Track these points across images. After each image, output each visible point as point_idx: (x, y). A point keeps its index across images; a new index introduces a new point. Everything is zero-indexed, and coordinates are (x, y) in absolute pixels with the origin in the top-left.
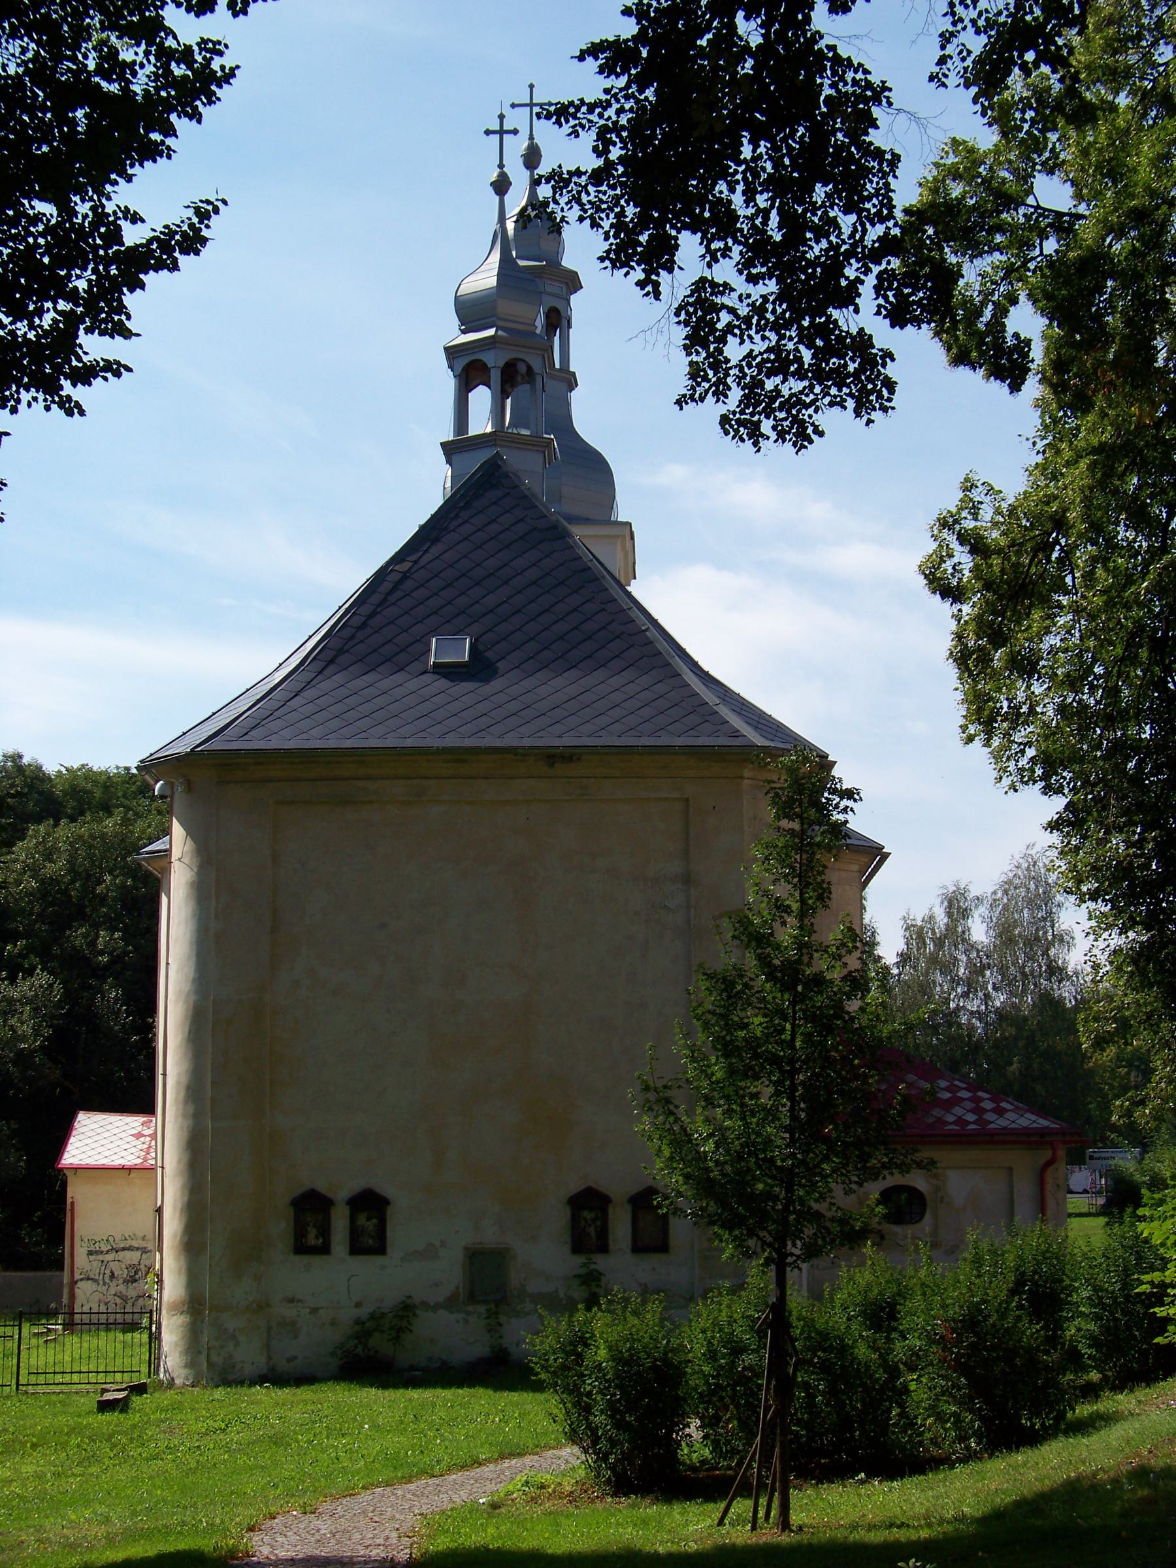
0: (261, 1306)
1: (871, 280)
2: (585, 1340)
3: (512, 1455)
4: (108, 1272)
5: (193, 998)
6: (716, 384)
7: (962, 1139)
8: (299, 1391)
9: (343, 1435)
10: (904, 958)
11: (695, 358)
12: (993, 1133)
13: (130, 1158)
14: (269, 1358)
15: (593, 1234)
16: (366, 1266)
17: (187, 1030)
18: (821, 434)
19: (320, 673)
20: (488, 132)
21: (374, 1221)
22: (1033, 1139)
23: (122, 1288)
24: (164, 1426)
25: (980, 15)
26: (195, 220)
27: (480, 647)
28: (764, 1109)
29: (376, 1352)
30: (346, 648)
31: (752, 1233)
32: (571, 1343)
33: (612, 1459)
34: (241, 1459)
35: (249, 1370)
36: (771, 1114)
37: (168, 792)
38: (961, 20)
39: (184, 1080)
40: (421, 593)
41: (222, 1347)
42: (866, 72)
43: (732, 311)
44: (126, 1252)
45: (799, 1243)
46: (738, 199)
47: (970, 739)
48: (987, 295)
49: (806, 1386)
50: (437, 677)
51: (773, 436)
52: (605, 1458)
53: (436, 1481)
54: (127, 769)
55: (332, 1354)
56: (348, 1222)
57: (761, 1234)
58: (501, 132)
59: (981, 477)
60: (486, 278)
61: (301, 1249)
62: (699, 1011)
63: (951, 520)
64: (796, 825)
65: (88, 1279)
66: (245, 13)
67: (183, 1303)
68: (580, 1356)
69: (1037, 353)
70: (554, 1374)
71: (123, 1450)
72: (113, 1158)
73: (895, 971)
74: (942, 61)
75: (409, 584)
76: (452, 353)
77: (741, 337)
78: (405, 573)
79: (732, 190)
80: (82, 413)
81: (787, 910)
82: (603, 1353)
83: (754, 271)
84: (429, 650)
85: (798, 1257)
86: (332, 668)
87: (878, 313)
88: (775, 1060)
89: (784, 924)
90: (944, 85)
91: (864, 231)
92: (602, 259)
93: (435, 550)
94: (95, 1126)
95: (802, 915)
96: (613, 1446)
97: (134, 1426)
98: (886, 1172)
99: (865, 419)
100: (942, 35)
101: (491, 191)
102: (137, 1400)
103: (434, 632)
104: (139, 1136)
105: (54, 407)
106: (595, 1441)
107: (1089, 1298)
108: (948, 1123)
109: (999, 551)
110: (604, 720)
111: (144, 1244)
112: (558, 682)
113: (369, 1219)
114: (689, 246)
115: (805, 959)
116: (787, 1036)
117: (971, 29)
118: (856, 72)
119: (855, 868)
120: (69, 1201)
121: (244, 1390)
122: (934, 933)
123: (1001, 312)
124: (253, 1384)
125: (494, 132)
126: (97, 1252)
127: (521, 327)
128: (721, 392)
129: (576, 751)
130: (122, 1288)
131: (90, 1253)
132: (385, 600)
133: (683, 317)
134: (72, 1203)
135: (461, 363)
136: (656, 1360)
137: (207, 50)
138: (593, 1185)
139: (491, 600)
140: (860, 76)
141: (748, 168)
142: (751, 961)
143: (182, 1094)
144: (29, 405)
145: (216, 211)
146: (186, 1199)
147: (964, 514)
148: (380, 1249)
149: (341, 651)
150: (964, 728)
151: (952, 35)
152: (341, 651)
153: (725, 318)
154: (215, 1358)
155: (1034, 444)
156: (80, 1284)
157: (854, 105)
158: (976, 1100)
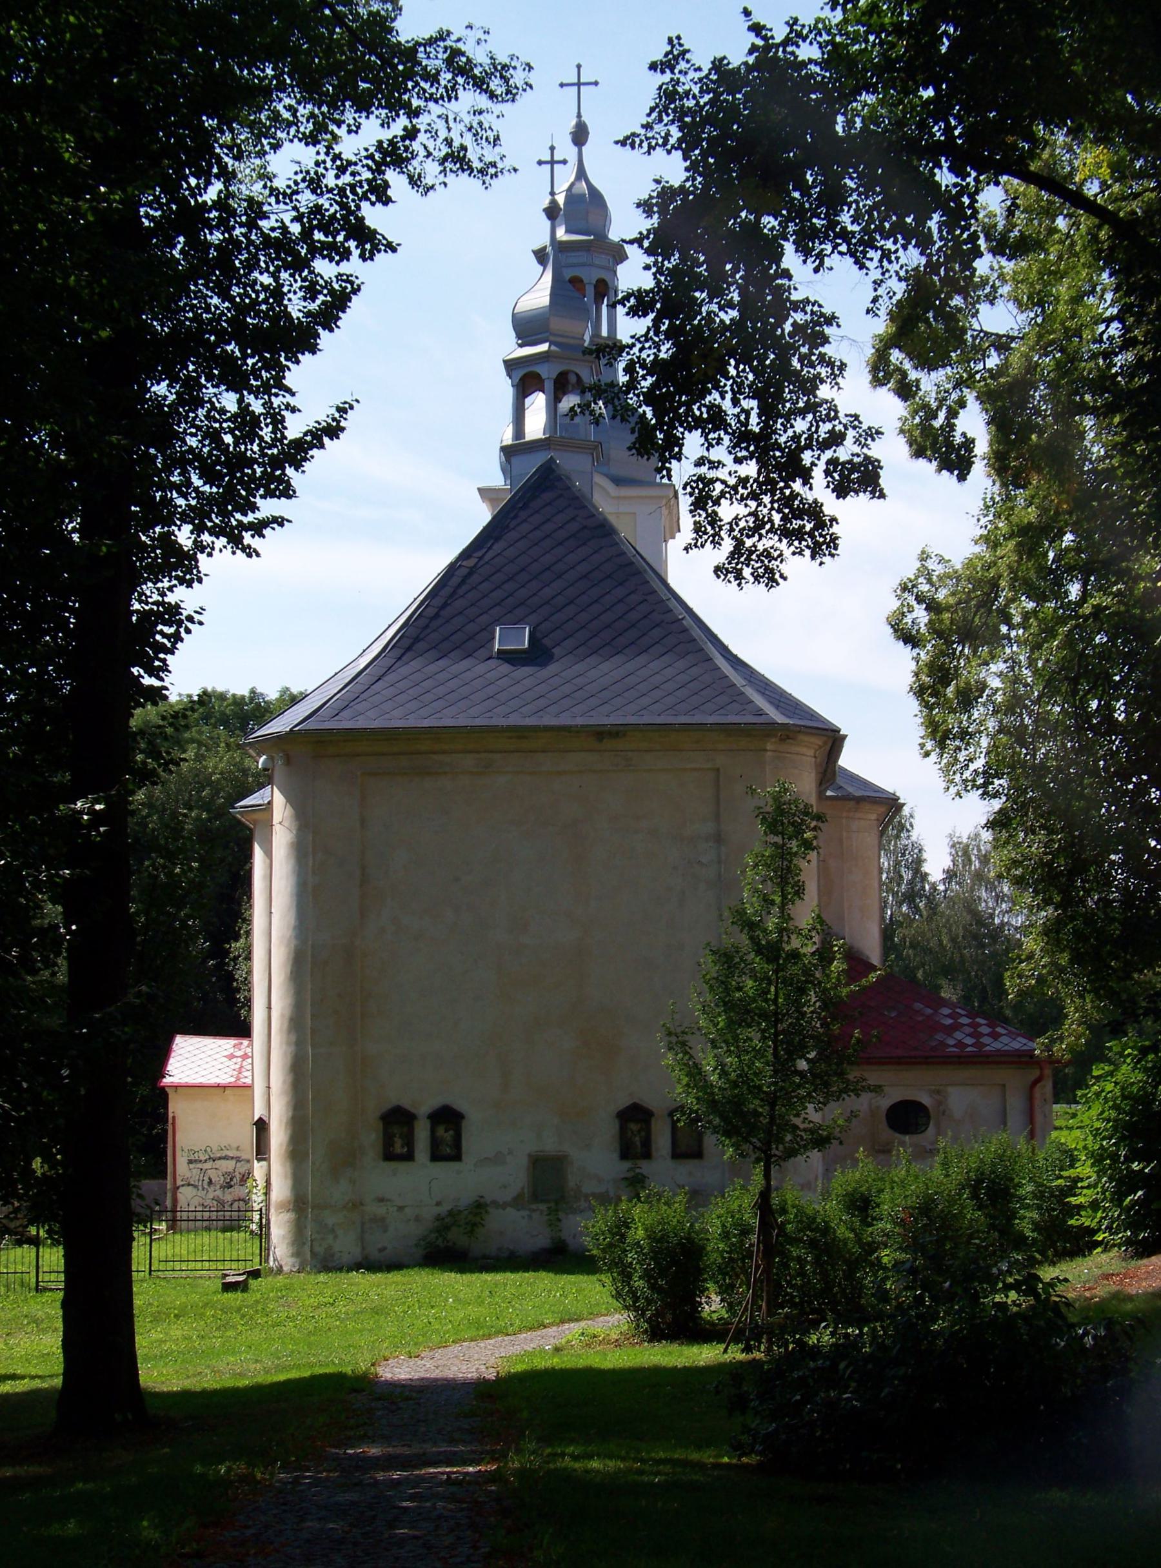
0: (356, 1205)
1: (822, 465)
2: (625, 1224)
3: (570, 1320)
4: (206, 1179)
5: (294, 942)
6: (714, 536)
7: (963, 1060)
8: (390, 1275)
9: (432, 1307)
10: (950, 875)
11: (697, 518)
12: (988, 1055)
13: (224, 1077)
14: (363, 1248)
15: (638, 1144)
16: (443, 1170)
17: (289, 971)
18: (785, 579)
19: (400, 658)
20: (540, 163)
21: (451, 1132)
22: (1023, 1059)
23: (219, 1193)
24: (282, 1301)
25: (901, 267)
26: (337, 415)
27: (538, 635)
28: (754, 1049)
29: (454, 1244)
30: (421, 636)
31: (746, 1140)
32: (617, 1227)
33: (648, 1313)
34: (350, 1325)
35: (346, 1259)
36: (759, 1054)
37: (270, 766)
38: (888, 271)
39: (288, 1013)
40: (485, 586)
41: (323, 1239)
42: (820, 306)
43: (724, 482)
44: (223, 1162)
45: (781, 1147)
46: (727, 405)
47: (927, 754)
48: (941, 401)
49: (799, 1259)
50: (500, 662)
51: (752, 579)
52: (643, 1315)
53: (511, 1338)
54: (190, 696)
55: (417, 1245)
56: (429, 1133)
57: (754, 1140)
58: (552, 162)
59: (933, 550)
60: (539, 296)
61: (389, 1156)
62: (708, 977)
63: (910, 585)
64: (778, 839)
65: (189, 1185)
66: (372, 260)
67: (289, 1202)
68: (623, 1237)
69: (982, 447)
70: (604, 1251)
71: (251, 1318)
72: (209, 1076)
73: (941, 888)
74: (875, 300)
75: (475, 578)
76: (511, 365)
77: (731, 499)
78: (471, 568)
79: (723, 398)
80: (258, 555)
81: (773, 903)
82: (641, 1233)
83: (739, 455)
84: (494, 638)
85: (780, 1157)
86: (409, 655)
87: (828, 486)
88: (764, 1015)
89: (769, 913)
90: (877, 315)
91: (818, 427)
92: (630, 449)
93: (498, 548)
94: (191, 1048)
95: (782, 907)
96: (648, 1304)
97: (257, 1302)
98: (844, 1095)
99: (818, 561)
100: (875, 282)
101: (543, 216)
102: (253, 1283)
103: (497, 622)
104: (231, 1057)
105: (238, 552)
106: (636, 1299)
107: (1033, 1192)
108: (949, 1046)
109: (947, 608)
110: (645, 701)
111: (238, 1154)
112: (606, 666)
113: (446, 1131)
114: (693, 443)
115: (785, 938)
116: (771, 996)
117: (895, 278)
118: (813, 305)
119: (874, 817)
120: (171, 1115)
121: (343, 1275)
122: (979, 850)
123: (952, 414)
124: (349, 1270)
125: (546, 163)
126: (196, 1161)
127: (572, 341)
128: (716, 542)
129: (622, 728)
130: (219, 1193)
131: (190, 1162)
132: (454, 592)
133: (689, 489)
134: (174, 1118)
135: (519, 374)
136: (682, 1238)
137: (342, 281)
138: (637, 1101)
139: (548, 592)
140: (816, 308)
141: (735, 382)
142: (744, 939)
143: (286, 1025)
144: (221, 551)
145: (351, 407)
146: (290, 1114)
147: (921, 580)
148: (457, 1157)
149: (417, 640)
150: (922, 746)
151: (882, 281)
152: (417, 640)
153: (719, 487)
154: (317, 1249)
155: (978, 520)
156: (181, 1190)
157: (812, 328)
158: (975, 1026)
